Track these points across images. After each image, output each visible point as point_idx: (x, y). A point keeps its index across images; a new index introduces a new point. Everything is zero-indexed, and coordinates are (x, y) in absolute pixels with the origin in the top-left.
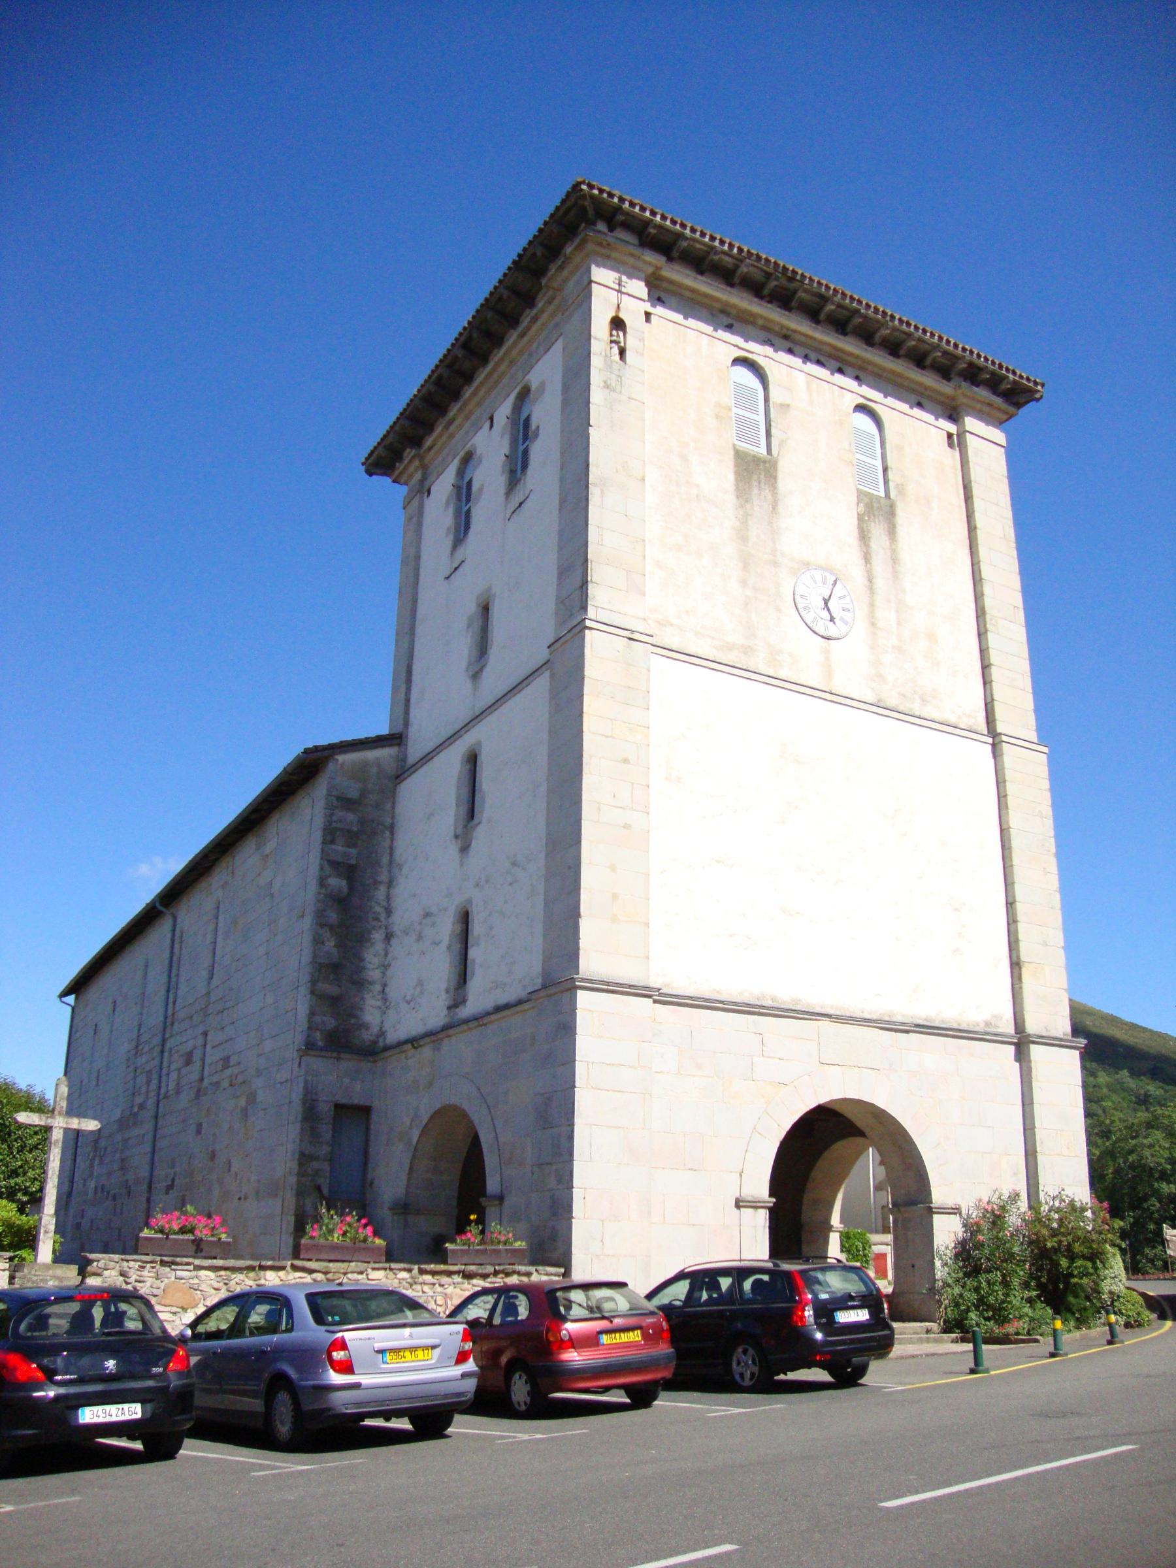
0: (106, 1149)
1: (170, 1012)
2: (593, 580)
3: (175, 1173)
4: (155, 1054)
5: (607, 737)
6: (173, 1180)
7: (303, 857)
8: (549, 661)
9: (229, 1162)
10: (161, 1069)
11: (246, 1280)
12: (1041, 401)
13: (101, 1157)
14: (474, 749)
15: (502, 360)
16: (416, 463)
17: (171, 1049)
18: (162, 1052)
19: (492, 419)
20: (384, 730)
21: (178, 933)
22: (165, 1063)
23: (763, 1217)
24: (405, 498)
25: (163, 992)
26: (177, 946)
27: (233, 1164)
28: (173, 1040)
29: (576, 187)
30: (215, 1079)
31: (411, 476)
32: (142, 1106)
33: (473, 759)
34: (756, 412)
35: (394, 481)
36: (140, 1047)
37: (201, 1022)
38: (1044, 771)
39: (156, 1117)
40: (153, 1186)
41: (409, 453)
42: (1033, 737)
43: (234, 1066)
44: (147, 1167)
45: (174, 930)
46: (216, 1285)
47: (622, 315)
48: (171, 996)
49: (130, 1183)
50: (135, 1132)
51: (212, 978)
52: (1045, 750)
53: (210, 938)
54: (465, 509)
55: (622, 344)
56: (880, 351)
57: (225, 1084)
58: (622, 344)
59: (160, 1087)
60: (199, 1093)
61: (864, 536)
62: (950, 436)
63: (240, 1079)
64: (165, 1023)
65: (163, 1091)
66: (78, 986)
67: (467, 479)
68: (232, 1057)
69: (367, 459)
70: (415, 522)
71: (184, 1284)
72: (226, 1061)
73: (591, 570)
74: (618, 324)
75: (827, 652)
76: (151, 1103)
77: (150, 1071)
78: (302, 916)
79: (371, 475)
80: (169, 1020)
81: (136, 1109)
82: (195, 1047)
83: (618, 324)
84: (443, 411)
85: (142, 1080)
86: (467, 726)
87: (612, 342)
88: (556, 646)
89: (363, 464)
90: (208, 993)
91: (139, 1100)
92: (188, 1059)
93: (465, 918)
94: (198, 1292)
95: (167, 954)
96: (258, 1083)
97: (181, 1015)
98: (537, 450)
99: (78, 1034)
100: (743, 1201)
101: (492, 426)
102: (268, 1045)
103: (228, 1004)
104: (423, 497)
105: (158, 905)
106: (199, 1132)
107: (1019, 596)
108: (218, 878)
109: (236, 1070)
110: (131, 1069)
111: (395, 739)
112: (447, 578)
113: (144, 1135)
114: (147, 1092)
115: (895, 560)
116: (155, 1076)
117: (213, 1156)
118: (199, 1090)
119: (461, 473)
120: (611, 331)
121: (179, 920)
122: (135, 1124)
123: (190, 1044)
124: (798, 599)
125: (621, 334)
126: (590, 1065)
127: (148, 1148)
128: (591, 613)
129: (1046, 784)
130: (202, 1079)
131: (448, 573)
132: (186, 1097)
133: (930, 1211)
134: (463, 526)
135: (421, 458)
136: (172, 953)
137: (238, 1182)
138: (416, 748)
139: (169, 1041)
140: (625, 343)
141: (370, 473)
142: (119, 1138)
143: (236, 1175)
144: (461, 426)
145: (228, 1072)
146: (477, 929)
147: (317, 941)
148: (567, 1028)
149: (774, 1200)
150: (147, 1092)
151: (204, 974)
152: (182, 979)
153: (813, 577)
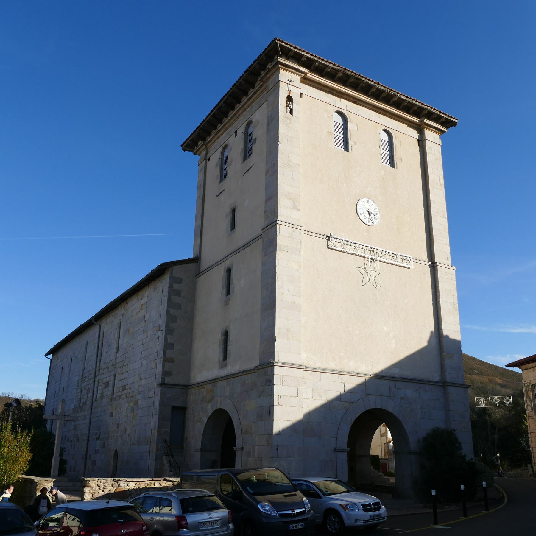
1: (98, 365)
3: (100, 433)
4: (91, 382)
6: (99, 435)
7: (159, 306)
9: (126, 429)
14: (229, 267)
15: (240, 109)
16: (204, 147)
18: (94, 381)
19: (236, 132)
20: (191, 256)
21: (101, 333)
22: (96, 386)
24: (199, 161)
25: (95, 356)
27: (127, 429)
28: (99, 376)
30: (120, 394)
31: (201, 152)
32: (85, 404)
35: (194, 154)
36: (84, 379)
37: (113, 370)
39: (92, 408)
40: (90, 437)
41: (200, 143)
42: (450, 263)
43: (127, 389)
45: (100, 332)
48: (99, 359)
51: (118, 352)
53: (116, 336)
54: (224, 168)
55: (291, 107)
56: (77, 497)
57: (124, 396)
59: (93, 396)
63: (131, 395)
64: (96, 369)
65: (95, 397)
66: (54, 351)
67: (225, 156)
68: (127, 386)
72: (124, 388)
73: (279, 200)
74: (289, 99)
76: (89, 402)
77: (89, 389)
79: (185, 151)
80: (98, 369)
81: (82, 404)
83: (289, 99)
84: (215, 127)
85: (84, 392)
88: (264, 230)
89: (181, 146)
90: (116, 358)
91: (83, 401)
92: (107, 385)
93: (226, 334)
95: (97, 341)
97: (103, 366)
98: (255, 149)
99: (54, 371)
101: (236, 136)
102: (143, 382)
104: (207, 161)
106: (112, 416)
108: (120, 311)
109: (129, 391)
110: (80, 387)
111: (196, 260)
112: (217, 196)
114: (87, 397)
116: (91, 391)
118: (112, 398)
119: (223, 153)
120: (287, 101)
121: (102, 327)
123: (108, 379)
126: (279, 396)
127: (88, 421)
128: (279, 218)
130: (113, 394)
132: (105, 401)
134: (223, 176)
135: (206, 145)
137: (130, 437)
138: (205, 263)
139: (97, 377)
143: (129, 434)
144: (222, 134)
145: (125, 392)
146: (231, 338)
148: (270, 382)
150: (87, 397)
151: (114, 351)
152: (104, 352)
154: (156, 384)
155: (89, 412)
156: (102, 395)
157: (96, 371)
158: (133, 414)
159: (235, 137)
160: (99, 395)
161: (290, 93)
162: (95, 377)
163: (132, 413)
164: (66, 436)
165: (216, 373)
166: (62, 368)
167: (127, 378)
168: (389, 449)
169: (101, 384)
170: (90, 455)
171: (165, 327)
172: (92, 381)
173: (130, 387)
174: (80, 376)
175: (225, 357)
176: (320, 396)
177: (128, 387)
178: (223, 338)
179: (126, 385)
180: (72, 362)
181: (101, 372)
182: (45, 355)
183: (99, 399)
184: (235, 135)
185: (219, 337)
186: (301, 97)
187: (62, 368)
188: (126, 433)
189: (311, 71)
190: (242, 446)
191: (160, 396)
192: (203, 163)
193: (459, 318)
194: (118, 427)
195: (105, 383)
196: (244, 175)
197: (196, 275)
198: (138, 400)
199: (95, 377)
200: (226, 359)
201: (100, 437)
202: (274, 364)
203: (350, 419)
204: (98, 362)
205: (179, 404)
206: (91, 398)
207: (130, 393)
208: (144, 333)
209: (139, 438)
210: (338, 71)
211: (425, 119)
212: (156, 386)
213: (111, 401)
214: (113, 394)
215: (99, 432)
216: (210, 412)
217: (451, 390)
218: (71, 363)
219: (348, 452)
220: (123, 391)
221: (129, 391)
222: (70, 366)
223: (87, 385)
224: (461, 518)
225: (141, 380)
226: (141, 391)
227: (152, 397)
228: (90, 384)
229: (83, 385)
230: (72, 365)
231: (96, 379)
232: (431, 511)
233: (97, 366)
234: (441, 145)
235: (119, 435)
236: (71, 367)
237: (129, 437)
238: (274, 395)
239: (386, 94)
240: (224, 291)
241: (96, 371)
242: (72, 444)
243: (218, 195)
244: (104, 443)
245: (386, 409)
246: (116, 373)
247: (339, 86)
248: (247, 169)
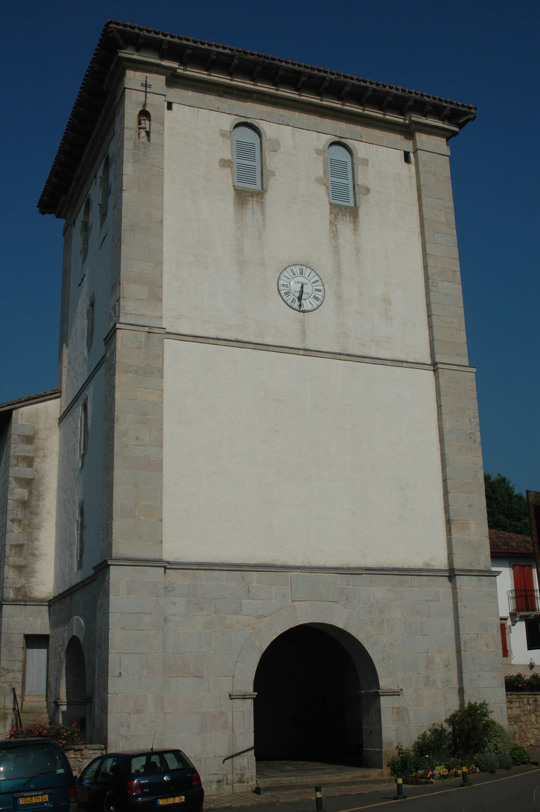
2: (124, 296)
12: (475, 120)
23: (249, 705)
29: (107, 26)
38: (473, 385)
42: (465, 361)
47: (147, 109)
52: (474, 370)
58: (148, 129)
61: (335, 235)
69: (39, 203)
70: (68, 243)
74: (144, 114)
75: (303, 324)
79: (43, 214)
83: (144, 114)
87: (140, 128)
88: (107, 340)
100: (233, 695)
107: (457, 263)
115: (358, 250)
124: (281, 288)
129: (474, 394)
133: (377, 696)
134: (85, 251)
140: (150, 129)
149: (256, 693)
153: (292, 271)
189: (183, 63)
193: (483, 457)
202: (109, 563)
210: (232, 57)
211: (412, 115)
219: (254, 699)
232: (21, 799)
234: (450, 155)
238: (110, 613)
239: (328, 83)
243: (81, 284)
247: (240, 80)
248: (103, 240)
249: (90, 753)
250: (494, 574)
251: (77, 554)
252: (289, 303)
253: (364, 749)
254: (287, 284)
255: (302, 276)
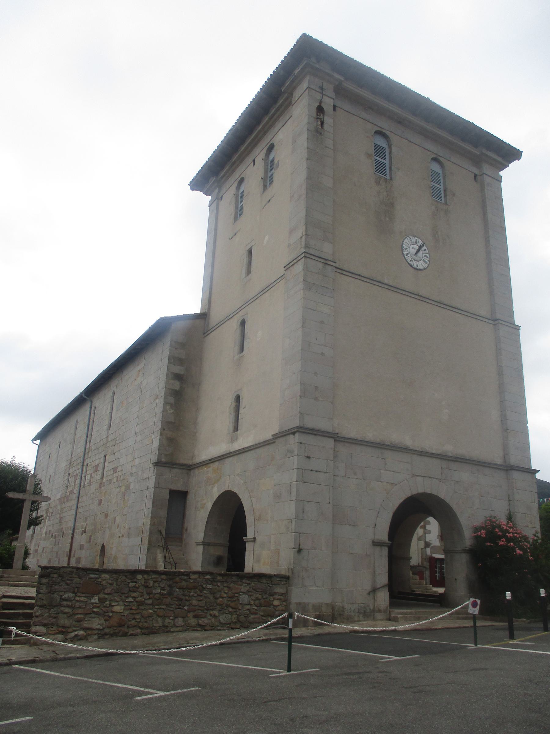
0: (52, 513)
1: (88, 447)
5: (314, 310)
6: (86, 528)
8: (284, 274)
10: (82, 474)
11: (127, 579)
13: (49, 517)
15: (260, 131)
17: (87, 465)
18: (83, 466)
19: (254, 161)
25: (84, 437)
26: (92, 415)
30: (110, 478)
32: (71, 492)
33: (243, 323)
34: (384, 159)
39: (79, 498)
44: (73, 522)
46: (110, 582)
47: (323, 105)
49: (64, 529)
50: (68, 504)
53: (109, 411)
54: (240, 206)
57: (115, 480)
58: (322, 120)
59: (81, 483)
60: (101, 485)
62: (475, 176)
63: (122, 478)
64: (85, 451)
65: (82, 484)
71: (93, 581)
72: (115, 470)
76: (76, 491)
77: (77, 475)
78: (156, 399)
80: (87, 451)
82: (100, 463)
85: (72, 479)
86: (240, 309)
87: (317, 118)
89: (189, 185)
90: (107, 437)
91: (70, 489)
93: (238, 399)
94: (101, 586)
95: (87, 419)
96: (131, 479)
98: (278, 175)
99: (41, 458)
101: (254, 164)
102: (137, 461)
103: (117, 442)
105: (83, 395)
106: (100, 504)
108: (114, 386)
109: (120, 474)
113: (72, 506)
114: (75, 485)
116: (79, 477)
117: (106, 516)
118: (101, 483)
119: (238, 188)
121: (93, 403)
122: (68, 501)
125: (322, 115)
127: (73, 512)
130: (102, 478)
131: (231, 237)
136: (90, 418)
138: (214, 319)
141: (193, 189)
142: (59, 507)
145: (115, 475)
146: (243, 403)
147: (164, 410)
150: (75, 485)
151: (106, 428)
152: (94, 430)
154: (151, 463)
155: (76, 502)
156: (90, 481)
157: (85, 454)
158: (124, 500)
159: (253, 166)
160: (87, 481)
161: (321, 102)
162: (84, 460)
163: (123, 500)
164: (50, 531)
165: (222, 448)
166: (50, 454)
167: (118, 459)
168: (427, 555)
169: (89, 468)
170: (75, 552)
171: (164, 394)
172: (80, 466)
173: (122, 469)
174: (68, 461)
175: (236, 429)
176: (355, 474)
177: (119, 469)
178: (234, 405)
179: (117, 467)
180: (60, 446)
181: (90, 454)
182: (32, 440)
183: (87, 486)
184: (253, 164)
185: (229, 402)
186: (335, 110)
187: (50, 454)
188: (115, 523)
190: (254, 536)
191: (155, 476)
192: (215, 203)
194: (106, 517)
195: (94, 467)
196: (263, 209)
197: (204, 334)
198: (130, 484)
199: (84, 460)
200: (237, 430)
201: (87, 529)
203: (392, 505)
204: (87, 443)
205: (179, 487)
206: (78, 485)
207: (122, 476)
208: (139, 403)
209: (130, 528)
212: (151, 465)
213: (100, 487)
214: (103, 478)
215: (85, 525)
216: (216, 495)
217: (516, 475)
218: (59, 447)
220: (113, 474)
221: (120, 474)
222: (58, 451)
223: (74, 471)
224: (506, 641)
225: (134, 459)
226: (133, 472)
227: (146, 478)
228: (78, 469)
229: (71, 471)
230: (60, 450)
231: (84, 463)
232: (506, 624)
233: (87, 448)
235: (107, 526)
236: (59, 451)
237: (118, 528)
240: (237, 348)
241: (85, 454)
242: (56, 540)
244: (91, 536)
245: (436, 495)
246: (106, 454)
249: (278, 580)
250: (534, 472)
251: (421, 591)
252: (408, 261)
253: (514, 623)
254: (407, 248)
255: (416, 244)
